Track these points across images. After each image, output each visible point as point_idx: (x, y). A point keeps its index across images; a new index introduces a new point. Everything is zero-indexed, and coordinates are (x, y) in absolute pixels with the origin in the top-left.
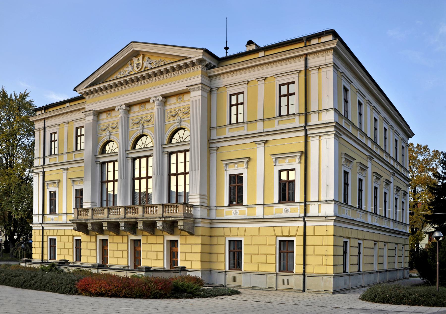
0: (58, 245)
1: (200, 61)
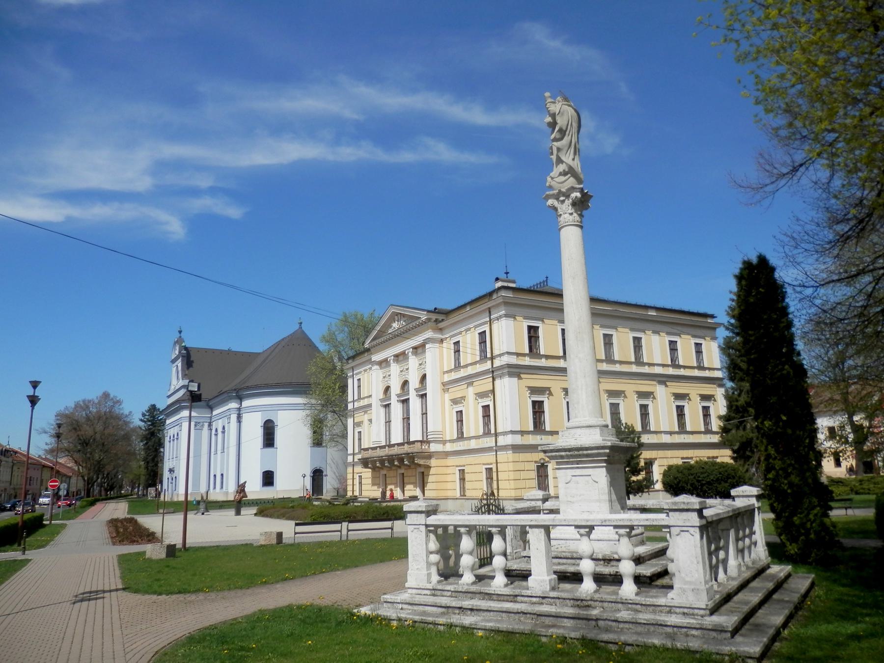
0: (467, 477)
1: (429, 320)
